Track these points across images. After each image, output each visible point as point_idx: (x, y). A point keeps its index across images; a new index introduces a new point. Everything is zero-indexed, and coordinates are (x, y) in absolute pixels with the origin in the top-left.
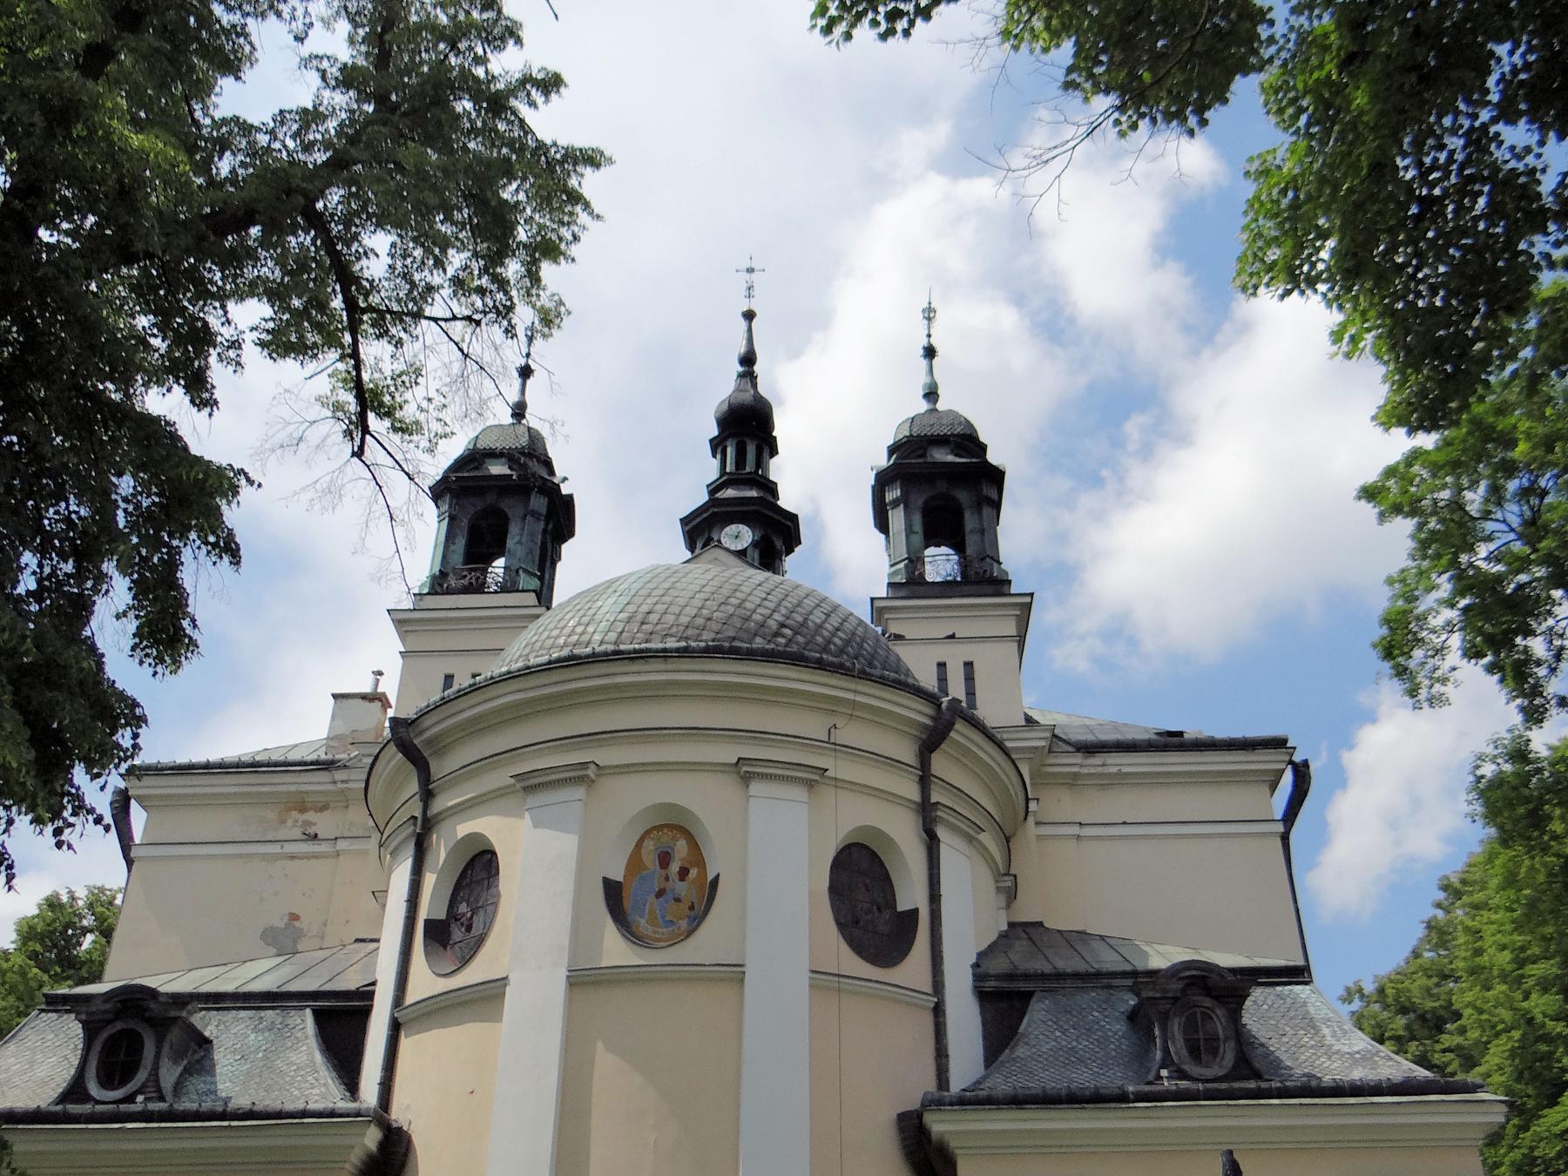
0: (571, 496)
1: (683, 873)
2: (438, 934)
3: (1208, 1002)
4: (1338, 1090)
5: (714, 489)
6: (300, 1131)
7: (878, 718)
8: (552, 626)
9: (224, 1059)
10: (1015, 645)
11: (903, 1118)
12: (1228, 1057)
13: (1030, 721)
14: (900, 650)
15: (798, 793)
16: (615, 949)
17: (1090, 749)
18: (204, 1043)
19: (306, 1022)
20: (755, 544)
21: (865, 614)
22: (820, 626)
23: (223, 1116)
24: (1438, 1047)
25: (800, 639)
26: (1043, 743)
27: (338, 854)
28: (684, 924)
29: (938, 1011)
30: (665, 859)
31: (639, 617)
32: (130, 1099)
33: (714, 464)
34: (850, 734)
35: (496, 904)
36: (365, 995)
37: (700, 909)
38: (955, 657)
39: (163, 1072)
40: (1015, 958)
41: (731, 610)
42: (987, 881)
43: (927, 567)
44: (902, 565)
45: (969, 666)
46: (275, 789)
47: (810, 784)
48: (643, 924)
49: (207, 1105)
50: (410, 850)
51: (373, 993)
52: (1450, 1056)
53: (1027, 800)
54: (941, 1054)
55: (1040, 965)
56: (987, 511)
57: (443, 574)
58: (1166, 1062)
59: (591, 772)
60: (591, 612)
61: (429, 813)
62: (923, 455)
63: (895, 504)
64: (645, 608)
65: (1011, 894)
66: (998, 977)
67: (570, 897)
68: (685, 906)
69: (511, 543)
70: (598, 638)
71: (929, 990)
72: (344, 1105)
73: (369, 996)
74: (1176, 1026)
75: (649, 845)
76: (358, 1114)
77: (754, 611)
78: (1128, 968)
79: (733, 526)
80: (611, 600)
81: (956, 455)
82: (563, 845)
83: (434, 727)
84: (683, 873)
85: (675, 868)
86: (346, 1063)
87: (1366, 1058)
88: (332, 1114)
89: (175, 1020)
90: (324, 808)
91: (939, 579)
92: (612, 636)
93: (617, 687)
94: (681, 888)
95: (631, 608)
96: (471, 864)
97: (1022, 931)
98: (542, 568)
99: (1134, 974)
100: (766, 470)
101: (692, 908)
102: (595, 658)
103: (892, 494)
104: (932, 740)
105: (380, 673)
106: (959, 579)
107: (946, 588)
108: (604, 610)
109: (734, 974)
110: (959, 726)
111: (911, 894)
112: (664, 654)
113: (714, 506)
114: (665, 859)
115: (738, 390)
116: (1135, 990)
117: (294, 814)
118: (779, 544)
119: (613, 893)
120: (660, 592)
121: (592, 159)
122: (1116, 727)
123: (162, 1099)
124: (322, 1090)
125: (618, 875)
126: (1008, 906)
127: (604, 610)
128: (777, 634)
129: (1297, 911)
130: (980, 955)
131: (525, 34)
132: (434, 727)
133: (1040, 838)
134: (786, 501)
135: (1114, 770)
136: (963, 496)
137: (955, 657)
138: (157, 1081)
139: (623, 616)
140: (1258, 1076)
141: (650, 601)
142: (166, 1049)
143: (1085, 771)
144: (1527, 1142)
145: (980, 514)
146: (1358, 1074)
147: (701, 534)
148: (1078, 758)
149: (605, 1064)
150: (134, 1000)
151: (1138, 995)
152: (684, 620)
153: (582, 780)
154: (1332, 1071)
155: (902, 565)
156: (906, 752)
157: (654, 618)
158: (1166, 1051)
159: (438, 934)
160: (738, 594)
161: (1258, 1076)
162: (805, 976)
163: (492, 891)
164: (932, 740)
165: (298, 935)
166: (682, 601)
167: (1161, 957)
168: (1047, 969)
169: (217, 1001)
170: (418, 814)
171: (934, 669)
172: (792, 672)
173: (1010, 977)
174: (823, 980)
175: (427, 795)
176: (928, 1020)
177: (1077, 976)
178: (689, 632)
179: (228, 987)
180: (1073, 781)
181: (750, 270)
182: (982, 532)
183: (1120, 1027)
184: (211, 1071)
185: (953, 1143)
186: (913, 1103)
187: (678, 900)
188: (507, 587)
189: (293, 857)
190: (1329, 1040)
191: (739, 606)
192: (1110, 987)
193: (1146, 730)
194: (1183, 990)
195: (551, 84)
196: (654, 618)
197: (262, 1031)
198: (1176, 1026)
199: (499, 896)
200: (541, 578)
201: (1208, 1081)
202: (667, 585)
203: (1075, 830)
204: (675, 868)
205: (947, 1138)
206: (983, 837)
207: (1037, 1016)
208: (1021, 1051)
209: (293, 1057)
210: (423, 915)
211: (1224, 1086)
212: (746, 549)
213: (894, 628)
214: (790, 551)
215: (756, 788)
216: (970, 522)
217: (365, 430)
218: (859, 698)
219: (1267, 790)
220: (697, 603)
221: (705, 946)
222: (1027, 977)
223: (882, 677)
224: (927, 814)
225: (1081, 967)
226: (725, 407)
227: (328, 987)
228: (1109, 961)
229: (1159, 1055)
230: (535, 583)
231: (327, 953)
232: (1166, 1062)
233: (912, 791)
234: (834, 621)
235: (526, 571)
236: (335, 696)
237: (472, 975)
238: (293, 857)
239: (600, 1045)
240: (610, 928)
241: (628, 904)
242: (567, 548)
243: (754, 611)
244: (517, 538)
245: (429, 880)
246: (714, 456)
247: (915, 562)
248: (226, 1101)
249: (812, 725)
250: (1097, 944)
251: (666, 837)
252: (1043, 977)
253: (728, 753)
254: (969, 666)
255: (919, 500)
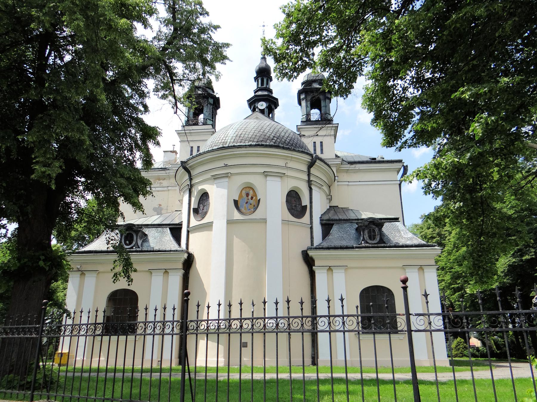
0: (219, 98)
1: (252, 198)
2: (196, 211)
3: (374, 227)
4: (402, 246)
5: (256, 92)
6: (169, 254)
7: (298, 160)
8: (217, 137)
9: (150, 238)
10: (334, 137)
11: (303, 252)
12: (378, 238)
13: (337, 156)
14: (304, 140)
15: (279, 179)
16: (237, 215)
17: (351, 163)
18: (146, 235)
19: (168, 230)
20: (267, 107)
21: (295, 130)
22: (283, 137)
23: (153, 251)
24: (443, 230)
25: (278, 140)
26: (340, 162)
27: (169, 190)
28: (252, 210)
29: (311, 228)
30: (247, 195)
31: (239, 135)
32: (132, 248)
33: (256, 84)
34: (291, 164)
35: (209, 205)
36: (180, 225)
37: (256, 206)
38: (318, 140)
39: (138, 242)
40: (330, 215)
41: (261, 133)
42: (324, 197)
43: (311, 116)
44: (305, 116)
45: (321, 142)
46: (154, 175)
47: (281, 177)
48: (243, 210)
49: (149, 249)
50: (188, 192)
51: (182, 224)
52: (447, 232)
53: (335, 177)
54: (312, 238)
55: (336, 217)
56: (327, 101)
57: (188, 120)
58: (363, 240)
59: (229, 175)
60: (227, 134)
61: (192, 184)
62: (311, 86)
63: (303, 99)
64: (240, 133)
65: (330, 200)
66: (326, 220)
67: (226, 204)
68: (252, 206)
69: (204, 112)
70: (229, 141)
71: (310, 224)
72: (179, 249)
73: (181, 225)
74: (366, 232)
75: (244, 192)
76: (182, 251)
77: (267, 133)
78: (357, 218)
79: (261, 102)
80: (232, 131)
81: (320, 85)
82: (224, 192)
83: (191, 163)
84: (252, 198)
85: (250, 197)
86: (177, 239)
87: (411, 239)
88: (177, 251)
89: (140, 231)
90: (164, 179)
91: (314, 120)
92: (232, 140)
93: (234, 154)
94: (251, 201)
95: (237, 133)
96: (202, 195)
97: (333, 208)
98: (213, 118)
99: (358, 220)
100: (269, 86)
101: (254, 206)
102: (229, 147)
103: (302, 96)
104: (311, 165)
105: (174, 145)
106: (320, 120)
107: (316, 122)
108: (230, 133)
109: (264, 221)
110: (318, 161)
111: (305, 201)
112: (245, 146)
113: (256, 97)
114: (247, 195)
115: (261, 63)
116: (357, 223)
117: (157, 181)
118: (273, 107)
119: (236, 202)
120: (244, 128)
121: (227, 45)
122: (359, 156)
123: (139, 247)
124: (172, 245)
125: (237, 199)
126: (330, 202)
127: (230, 133)
128: (273, 139)
129: (401, 202)
130: (322, 215)
131: (210, 14)
132: (191, 163)
133: (338, 185)
134: (274, 95)
135: (358, 168)
136: (321, 97)
137: (318, 140)
138: (137, 244)
139: (235, 135)
140: (384, 243)
141: (241, 131)
142: (138, 237)
143: (350, 169)
144: (458, 255)
145: (325, 102)
146: (409, 243)
147: (253, 104)
148: (349, 166)
149: (236, 241)
150: (130, 227)
151: (358, 225)
152: (250, 136)
153: (227, 177)
154: (402, 242)
155: (305, 116)
156: (305, 168)
157: (242, 136)
158: (364, 237)
159: (196, 211)
160: (263, 129)
161: (384, 243)
162: (280, 222)
163: (208, 202)
164: (311, 165)
165: (161, 209)
166: (249, 131)
167: (365, 215)
168: (337, 218)
169: (147, 226)
170: (189, 183)
171: (313, 143)
172: (276, 150)
173: (328, 220)
174: (284, 222)
175: (191, 179)
176: (309, 230)
177: (344, 220)
178: (251, 139)
179: (150, 223)
180: (347, 171)
181: (264, 26)
182: (326, 107)
183: (354, 232)
184: (148, 241)
185: (314, 257)
186: (305, 249)
187: (251, 204)
188: (205, 124)
189: (158, 191)
190: (403, 235)
191: (263, 132)
192: (352, 222)
193: (367, 157)
194: (369, 224)
195: (216, 27)
196: (242, 136)
197: (158, 232)
198: (366, 232)
199: (209, 203)
200: (213, 121)
201: (373, 244)
202: (245, 126)
203: (347, 183)
204: (250, 197)
205: (313, 256)
206: (323, 187)
207: (335, 230)
208: (330, 237)
209: (166, 238)
210: (192, 207)
211: (376, 245)
212: (264, 109)
213: (303, 133)
214: (276, 108)
215: (269, 178)
216: (323, 104)
217: (177, 108)
218: (293, 156)
219: (396, 173)
220: (253, 131)
221: (258, 214)
222: (332, 220)
223: (298, 150)
224: (309, 182)
225: (345, 218)
226: (258, 68)
227: (172, 223)
228: (352, 216)
229: (362, 238)
230: (211, 122)
231: (169, 214)
232: (363, 240)
233: (306, 178)
234: (287, 135)
235: (209, 119)
236: (164, 152)
237: (205, 221)
238: (158, 191)
239: (235, 236)
240: (236, 211)
241: (239, 205)
242: (219, 111)
243: (267, 133)
244: (206, 110)
245: (193, 199)
246: (255, 81)
247: (308, 115)
248: (153, 248)
249: (281, 163)
250: (350, 212)
251: (248, 190)
252: (336, 220)
253: (262, 170)
254: (321, 142)
255: (309, 98)
